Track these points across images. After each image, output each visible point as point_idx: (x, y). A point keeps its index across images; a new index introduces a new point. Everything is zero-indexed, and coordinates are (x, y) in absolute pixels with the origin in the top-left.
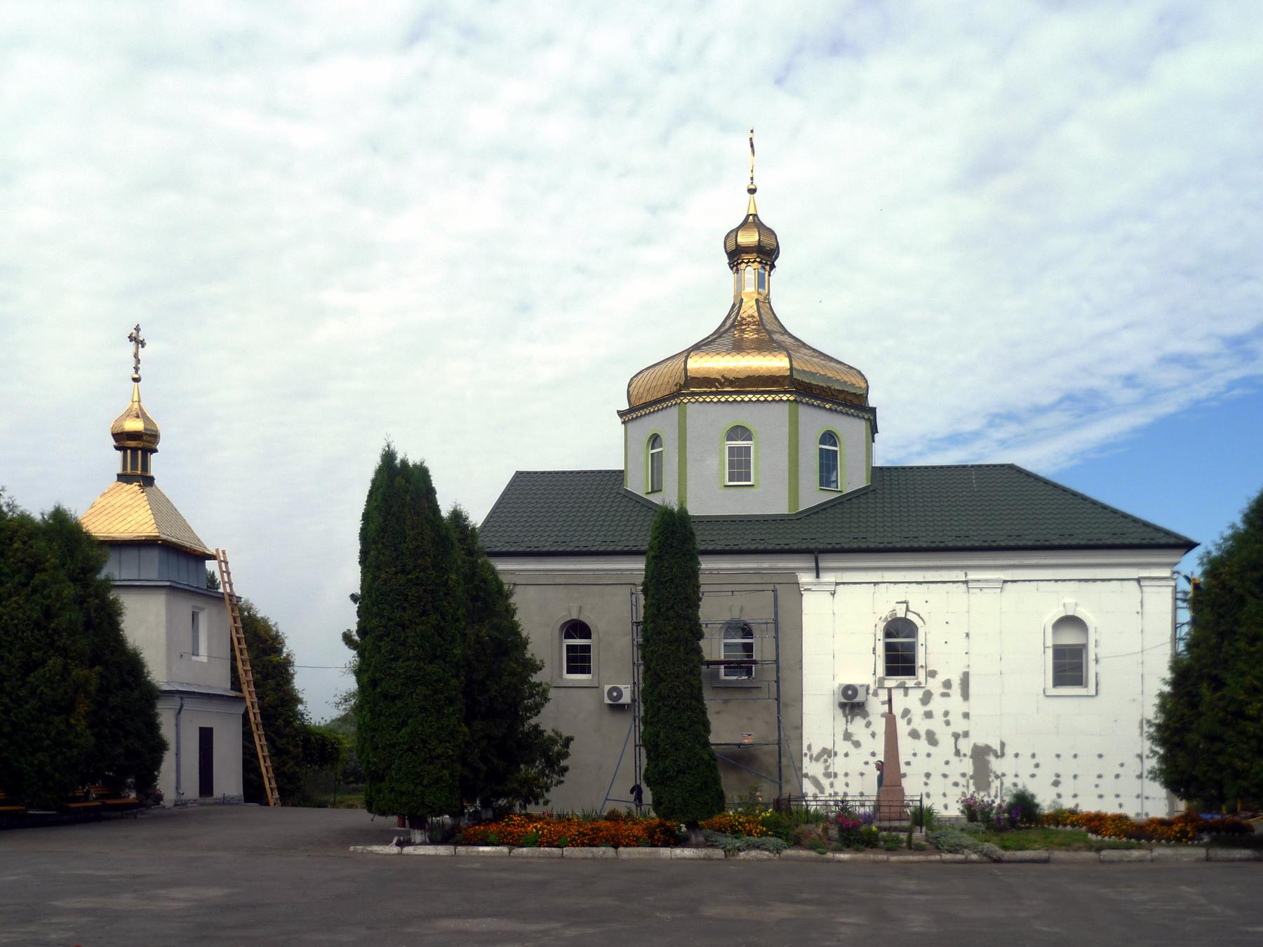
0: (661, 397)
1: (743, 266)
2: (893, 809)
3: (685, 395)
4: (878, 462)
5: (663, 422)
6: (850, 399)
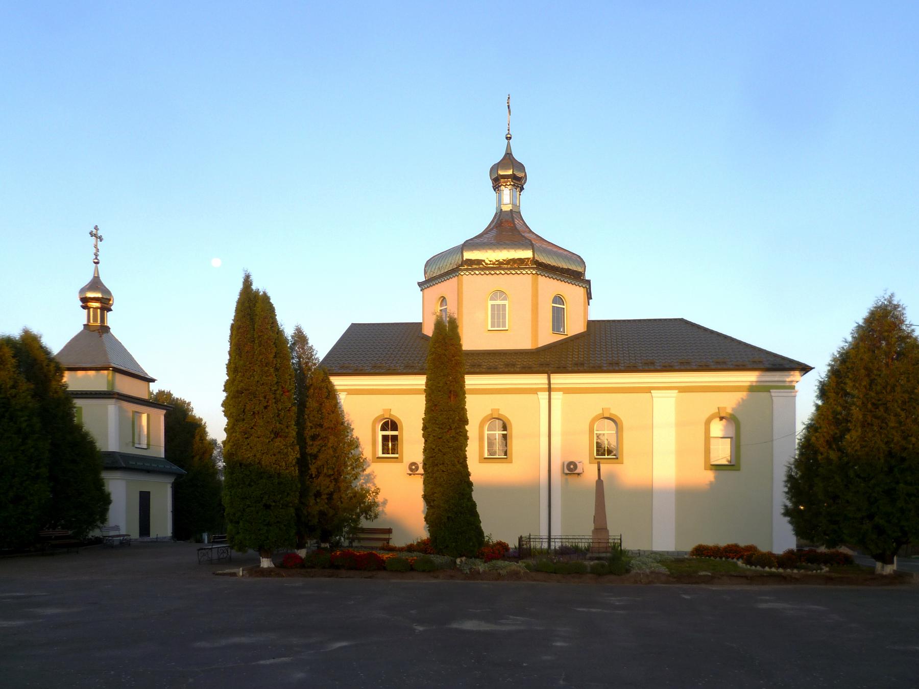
0: (443, 270)
1: (502, 188)
2: (601, 545)
3: (462, 270)
4: (593, 316)
5: (447, 288)
6: (572, 273)
